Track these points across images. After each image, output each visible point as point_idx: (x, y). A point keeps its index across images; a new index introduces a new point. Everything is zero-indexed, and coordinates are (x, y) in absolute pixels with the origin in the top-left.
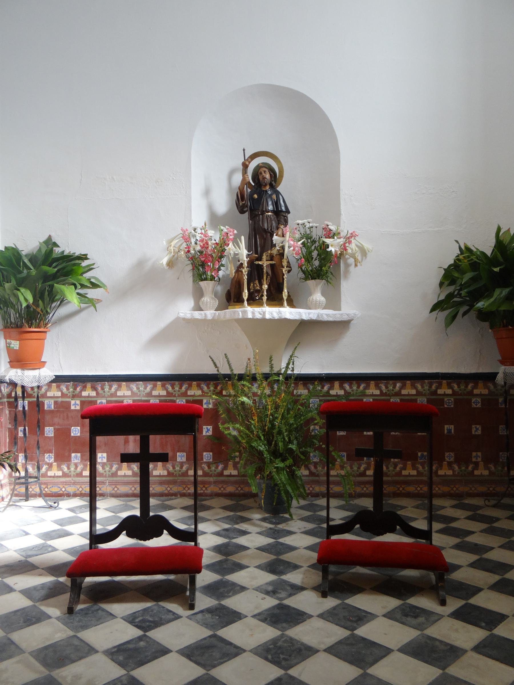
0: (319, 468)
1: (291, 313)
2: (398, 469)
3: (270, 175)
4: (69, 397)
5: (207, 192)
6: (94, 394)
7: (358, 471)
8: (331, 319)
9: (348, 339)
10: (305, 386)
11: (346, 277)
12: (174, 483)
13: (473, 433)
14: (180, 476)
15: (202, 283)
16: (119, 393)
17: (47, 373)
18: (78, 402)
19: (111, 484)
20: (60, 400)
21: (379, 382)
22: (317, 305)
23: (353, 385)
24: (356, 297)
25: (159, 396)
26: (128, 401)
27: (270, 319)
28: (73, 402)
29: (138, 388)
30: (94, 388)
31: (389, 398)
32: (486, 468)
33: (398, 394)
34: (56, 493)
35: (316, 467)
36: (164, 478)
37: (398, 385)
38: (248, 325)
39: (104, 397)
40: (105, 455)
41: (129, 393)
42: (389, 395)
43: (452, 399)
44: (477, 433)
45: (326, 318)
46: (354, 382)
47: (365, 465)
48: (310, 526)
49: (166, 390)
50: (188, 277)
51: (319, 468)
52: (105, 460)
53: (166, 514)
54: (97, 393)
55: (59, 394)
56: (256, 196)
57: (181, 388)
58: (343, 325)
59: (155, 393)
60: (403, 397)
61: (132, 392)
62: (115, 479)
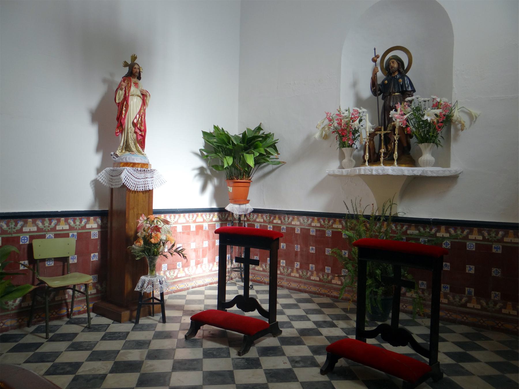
0: (426, 294)
1: (408, 171)
2: (498, 306)
3: (398, 64)
4: (267, 223)
5: (354, 84)
6: (279, 222)
7: (459, 302)
8: (435, 175)
9: (455, 191)
10: (417, 228)
11: (455, 140)
12: (323, 286)
13: (467, 271)
14: (326, 282)
15: (344, 149)
16: (293, 223)
17: (249, 207)
18: (271, 226)
19: (287, 280)
20: (263, 224)
21: (482, 229)
22: (427, 164)
23: (457, 230)
24: (462, 156)
25: (316, 227)
26: (382, 237)
27: (376, 175)
28: (269, 226)
29: (304, 221)
30: (280, 218)
31: (490, 243)
32: (478, 302)
33: (500, 241)
34: (259, 280)
35: (423, 293)
36: (317, 283)
37: (501, 233)
38: (369, 179)
39: (285, 224)
40: (284, 261)
41: (298, 223)
42: (491, 241)
43: (474, 244)
44: (470, 272)
45: (430, 174)
46: (459, 228)
47: (501, 304)
48: (497, 359)
49: (320, 223)
50: (337, 144)
51: (426, 294)
52: (284, 265)
53: (410, 329)
54: (281, 222)
55: (262, 220)
56: (386, 82)
57: (329, 222)
58: (453, 179)
59: (313, 224)
60: (505, 244)
61: (300, 223)
62: (289, 278)
